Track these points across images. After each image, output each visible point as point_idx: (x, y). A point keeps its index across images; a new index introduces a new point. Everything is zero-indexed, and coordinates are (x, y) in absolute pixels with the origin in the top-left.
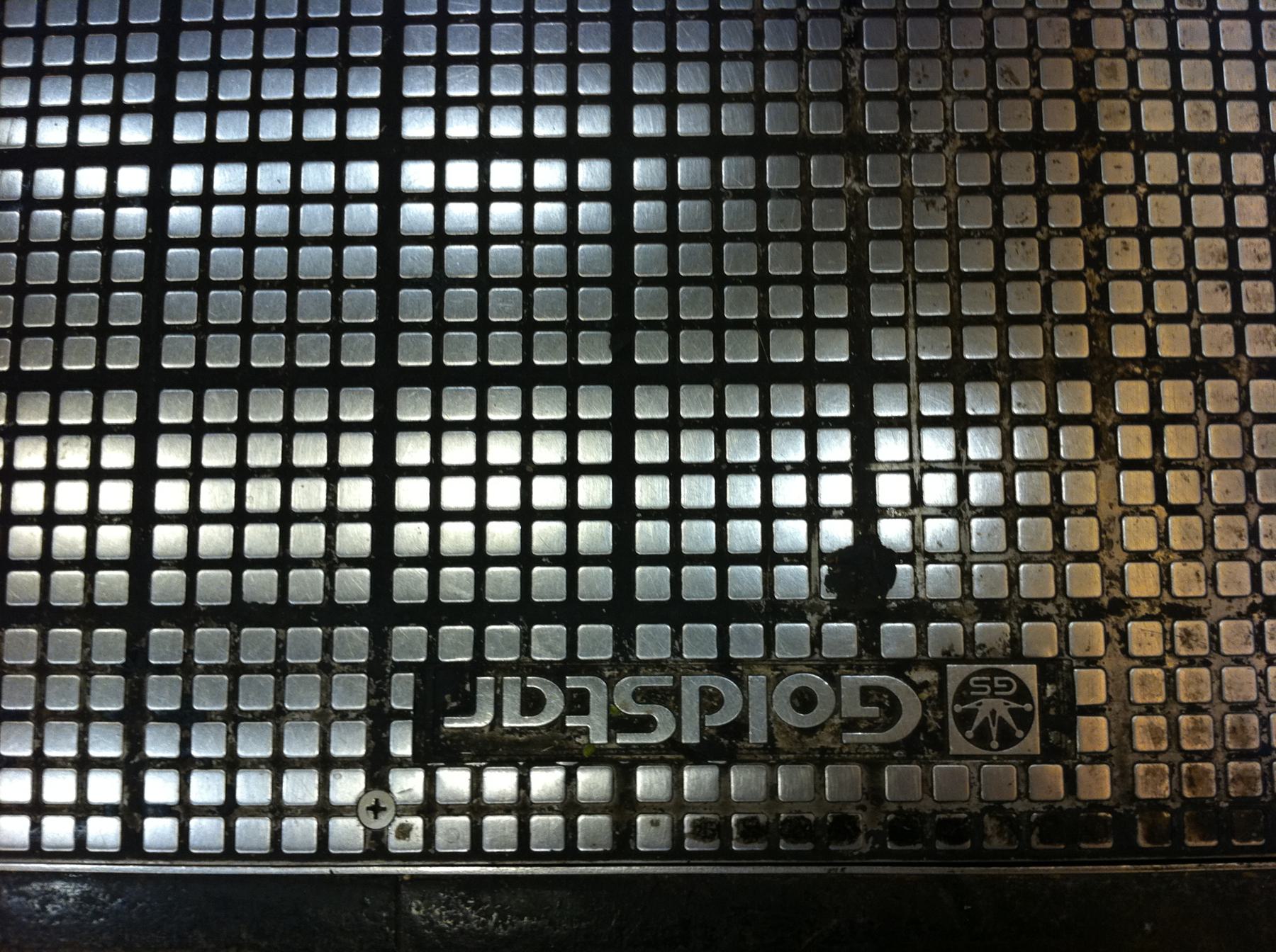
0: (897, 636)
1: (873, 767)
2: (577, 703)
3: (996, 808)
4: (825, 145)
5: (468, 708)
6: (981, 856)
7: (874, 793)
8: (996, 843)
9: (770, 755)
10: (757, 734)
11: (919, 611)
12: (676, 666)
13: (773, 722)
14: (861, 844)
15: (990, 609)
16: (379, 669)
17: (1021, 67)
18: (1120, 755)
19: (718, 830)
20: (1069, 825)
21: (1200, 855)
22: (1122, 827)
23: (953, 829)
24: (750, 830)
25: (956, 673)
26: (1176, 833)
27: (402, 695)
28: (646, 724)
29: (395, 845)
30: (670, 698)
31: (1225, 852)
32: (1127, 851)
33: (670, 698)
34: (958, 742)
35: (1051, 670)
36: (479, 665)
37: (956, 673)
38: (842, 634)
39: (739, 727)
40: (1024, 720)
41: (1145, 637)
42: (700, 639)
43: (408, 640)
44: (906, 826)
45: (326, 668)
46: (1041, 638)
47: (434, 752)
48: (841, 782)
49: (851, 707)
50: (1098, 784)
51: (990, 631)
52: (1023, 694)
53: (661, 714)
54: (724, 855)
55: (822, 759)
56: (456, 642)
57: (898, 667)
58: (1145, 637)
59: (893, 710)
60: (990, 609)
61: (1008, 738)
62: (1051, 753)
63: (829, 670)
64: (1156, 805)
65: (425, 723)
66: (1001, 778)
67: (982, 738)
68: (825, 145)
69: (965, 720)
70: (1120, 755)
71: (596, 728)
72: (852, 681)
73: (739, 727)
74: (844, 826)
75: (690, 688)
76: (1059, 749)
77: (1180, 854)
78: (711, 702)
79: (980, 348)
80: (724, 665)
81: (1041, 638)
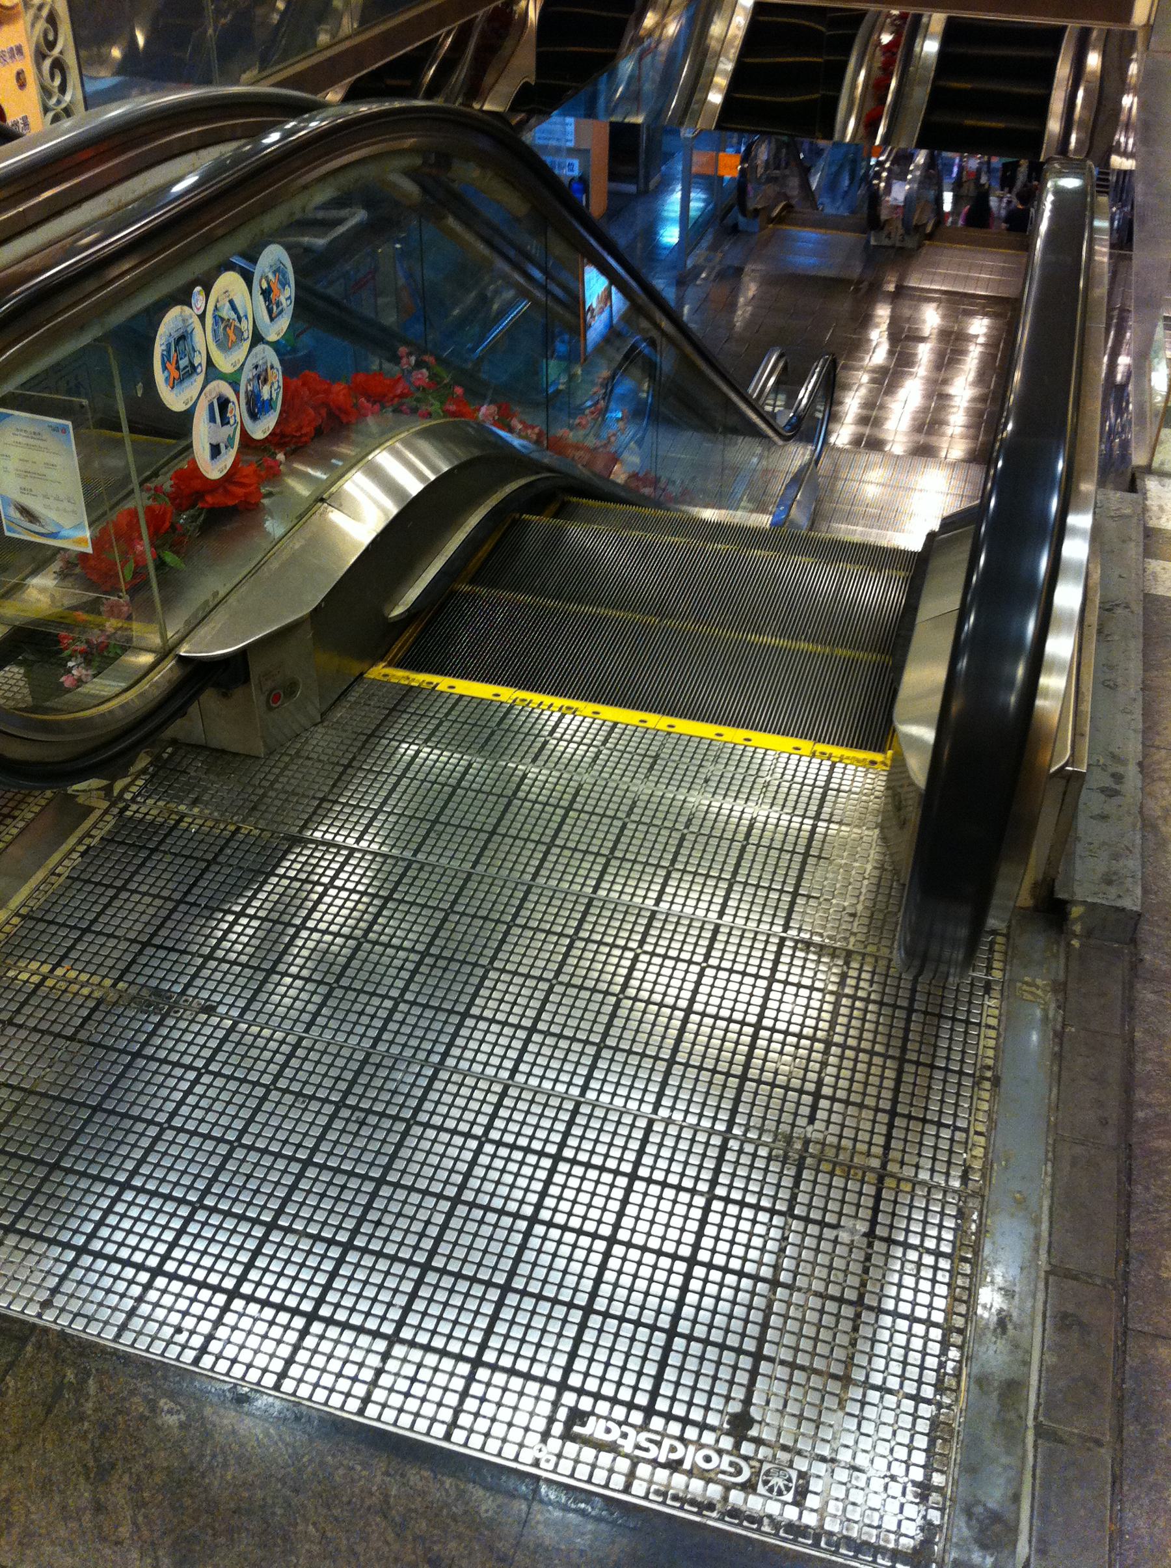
0: (747, 1448)
1: (728, 1488)
2: (624, 1436)
3: (770, 1516)
4: (835, 1377)
5: (583, 1424)
6: (758, 1530)
7: (725, 1499)
8: (766, 1529)
9: (690, 1473)
10: (687, 1465)
11: (758, 1442)
12: (663, 1434)
13: (694, 1464)
14: (714, 1514)
15: (785, 1448)
16: (556, 1404)
17: (841, 1275)
18: (821, 1512)
19: (664, 1494)
20: (796, 1530)
21: (784, 1540)
22: (817, 1538)
23: (752, 1519)
24: (675, 1498)
25: (766, 1466)
26: (838, 1546)
27: (562, 1414)
28: (651, 1441)
29: (543, 1464)
30: (658, 1444)
31: (795, 1542)
32: (816, 1545)
33: (658, 1444)
34: (761, 1489)
35: (802, 1475)
36: (592, 1413)
37: (766, 1466)
38: (727, 1443)
39: (680, 1462)
40: (788, 1489)
41: (842, 1475)
42: (675, 1428)
43: (569, 1398)
44: (735, 1513)
45: (537, 1398)
46: (801, 1464)
47: (567, 1436)
48: (715, 1491)
49: (725, 1466)
50: (810, 1519)
51: (783, 1456)
52: (790, 1480)
53: (653, 1447)
54: (664, 1503)
55: (708, 1481)
56: (586, 1404)
57: (746, 1459)
58: (842, 1475)
59: (739, 1472)
60: (785, 1448)
61: (780, 1493)
62: (795, 1503)
63: (720, 1452)
64: (831, 1534)
65: (569, 1424)
66: (773, 1508)
67: (771, 1490)
68: (835, 1377)
69: (766, 1483)
70: (821, 1512)
71: (628, 1446)
72: (726, 1459)
73: (680, 1462)
74: (711, 1506)
75: (667, 1443)
76: (799, 1502)
77: (836, 1553)
78: (673, 1449)
79: (803, 1359)
80: (681, 1439)
81: (801, 1464)
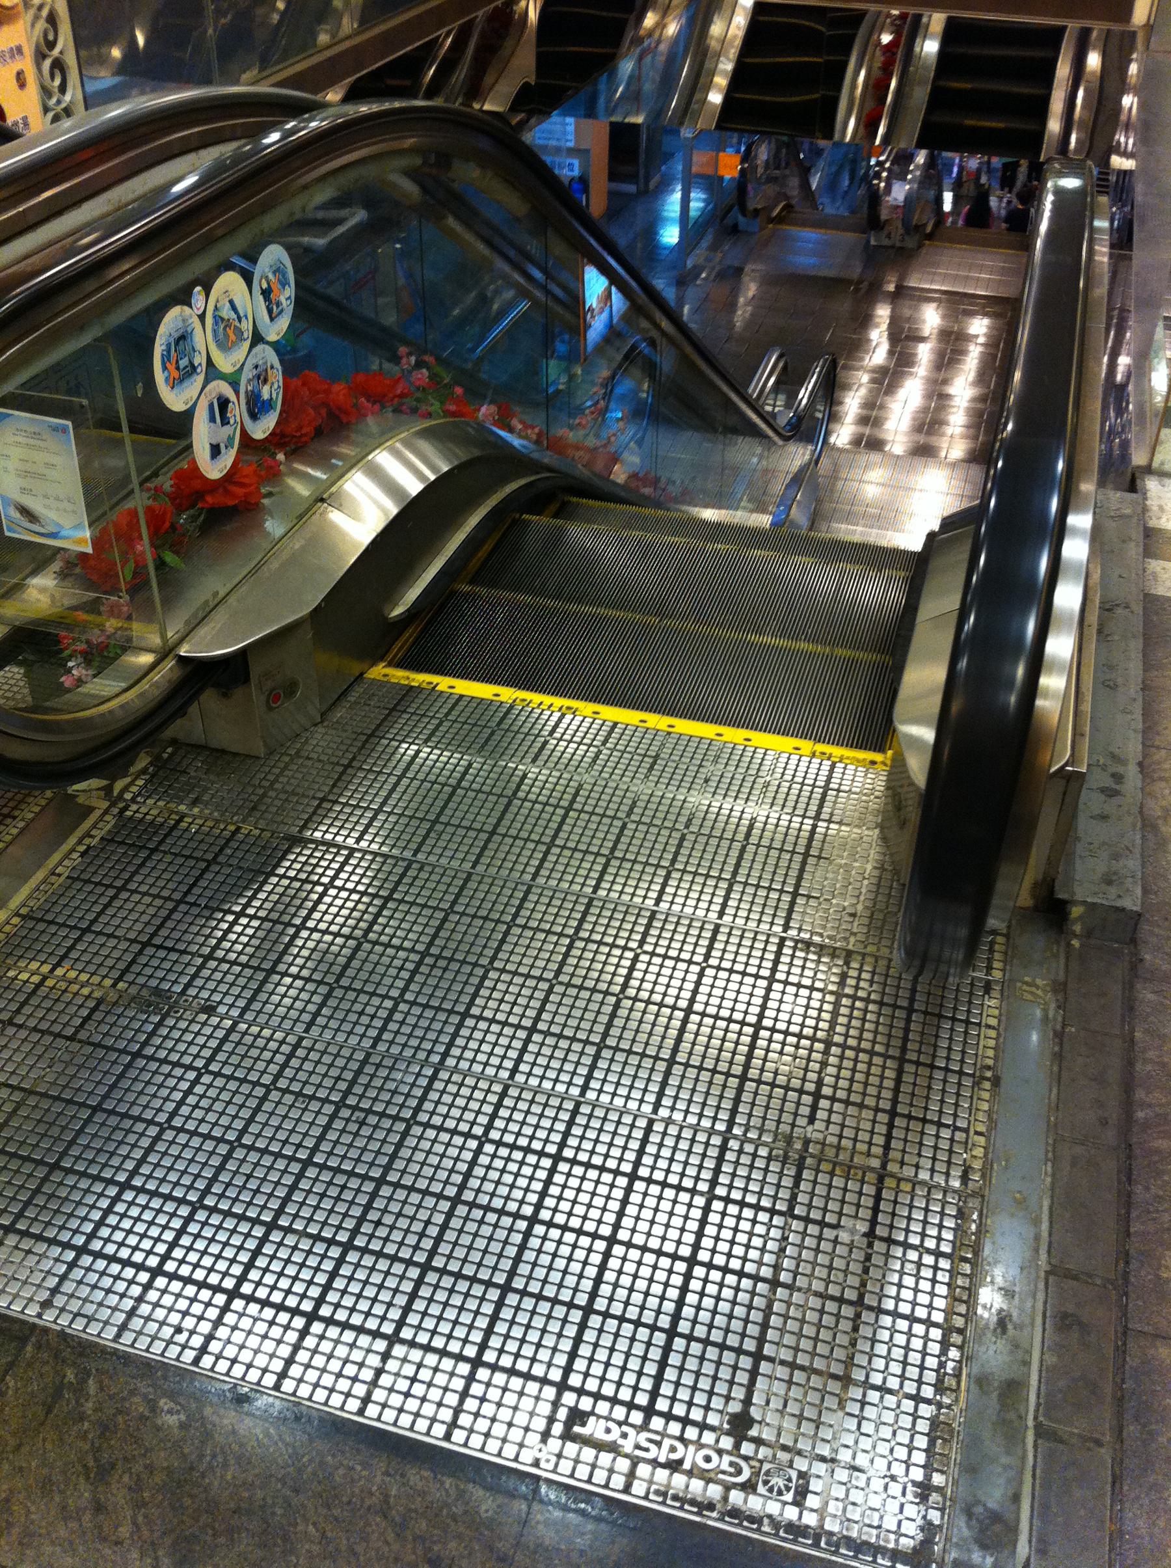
0: (747, 1448)
1: (728, 1488)
2: (624, 1436)
3: (770, 1516)
4: (835, 1377)
5: (583, 1424)
6: (758, 1530)
7: (725, 1499)
8: (766, 1529)
9: (690, 1473)
10: (687, 1465)
11: (758, 1442)
12: (663, 1434)
13: (694, 1464)
14: (714, 1514)
15: (785, 1448)
16: (556, 1404)
17: (841, 1275)
18: (821, 1512)
19: (664, 1494)
20: (796, 1530)
22: (817, 1538)
23: (752, 1519)
24: (675, 1498)
25: (766, 1466)
26: (838, 1546)
27: (562, 1414)
28: (651, 1441)
29: (543, 1464)
30: (658, 1444)
32: (816, 1545)
33: (658, 1444)
34: (761, 1489)
35: (802, 1475)
36: (592, 1413)
37: (766, 1466)
38: (727, 1443)
39: (680, 1462)
40: (788, 1489)
41: (842, 1475)
42: (675, 1428)
43: (569, 1398)
44: (735, 1513)
45: (537, 1398)
46: (801, 1464)
47: (567, 1436)
48: (715, 1491)
49: (725, 1466)
50: (810, 1519)
51: (783, 1456)
52: (790, 1480)
53: (653, 1447)
54: (664, 1503)
55: (708, 1481)
56: (586, 1404)
57: (746, 1459)
58: (842, 1475)
59: (739, 1472)
60: (785, 1448)
61: (780, 1493)
62: (795, 1503)
63: (720, 1452)
64: (831, 1534)
65: (569, 1424)
66: (773, 1508)
67: (771, 1490)
68: (835, 1377)
69: (766, 1483)
70: (821, 1512)
71: (628, 1446)
72: (726, 1459)
73: (680, 1462)
74: (711, 1506)
75: (667, 1443)
76: (799, 1502)
77: (836, 1553)
78: (673, 1449)
79: (803, 1359)
80: (681, 1439)
81: (801, 1464)
